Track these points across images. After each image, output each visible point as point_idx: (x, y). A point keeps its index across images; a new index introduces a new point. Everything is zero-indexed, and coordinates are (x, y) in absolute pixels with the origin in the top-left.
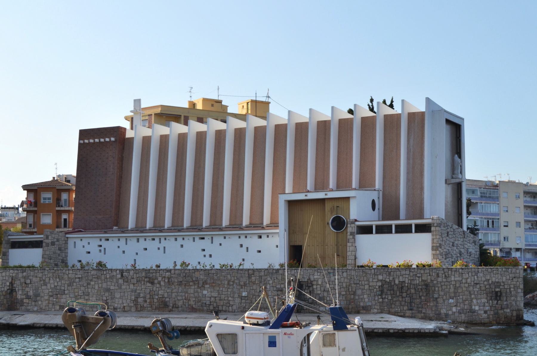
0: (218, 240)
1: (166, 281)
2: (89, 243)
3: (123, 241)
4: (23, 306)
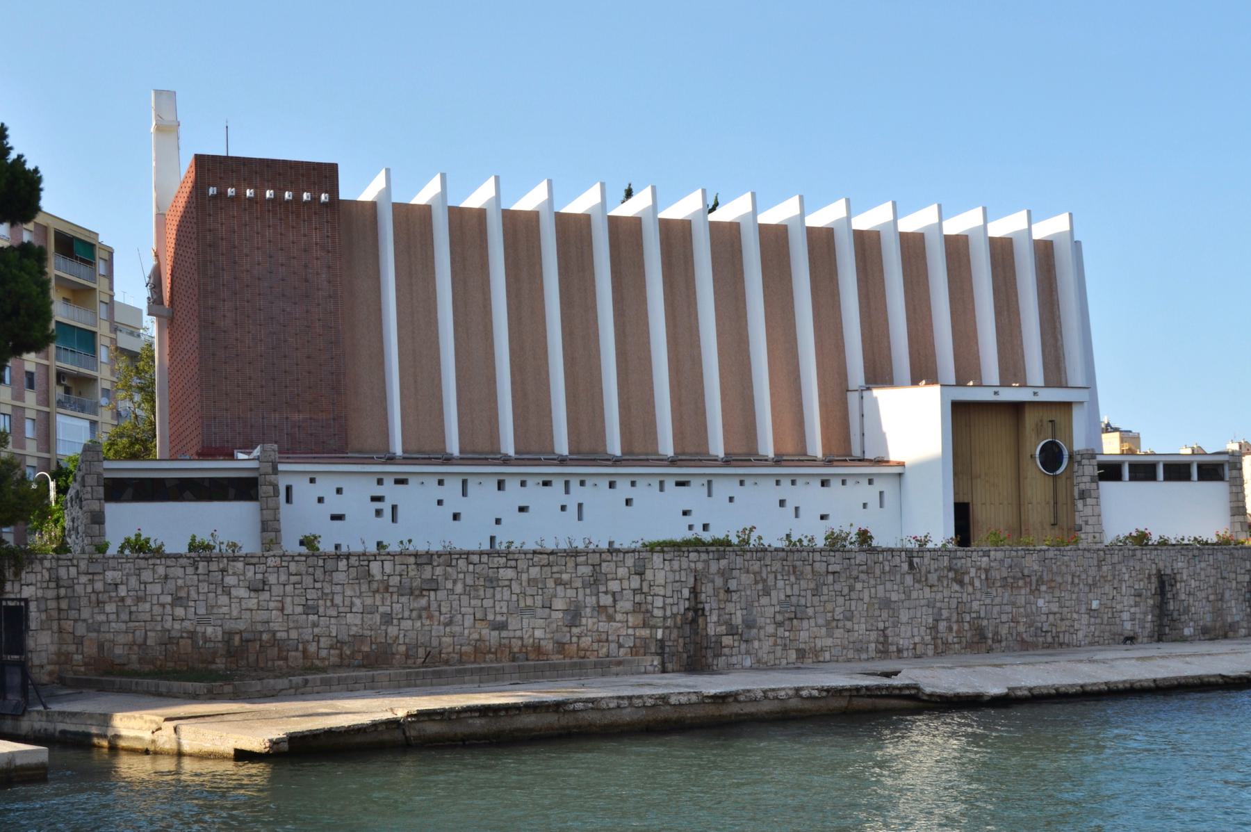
0: (724, 488)
1: (983, 577)
2: (339, 491)
3: (454, 485)
4: (720, 655)
